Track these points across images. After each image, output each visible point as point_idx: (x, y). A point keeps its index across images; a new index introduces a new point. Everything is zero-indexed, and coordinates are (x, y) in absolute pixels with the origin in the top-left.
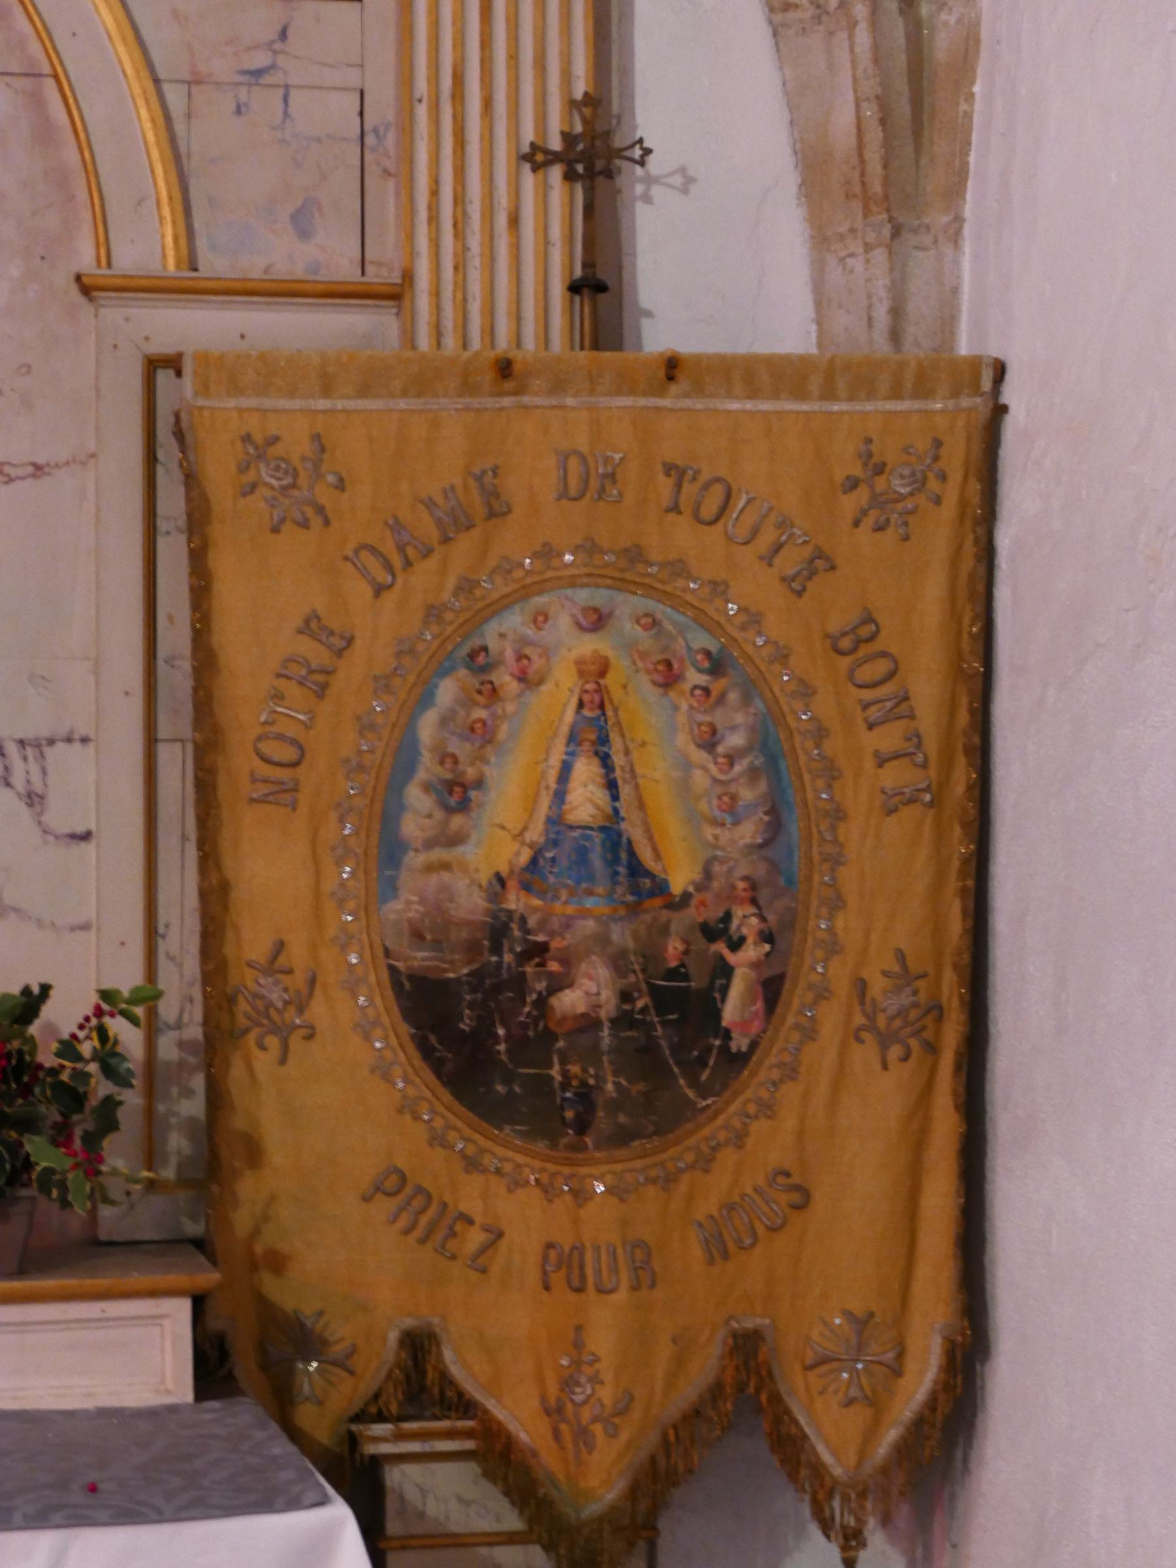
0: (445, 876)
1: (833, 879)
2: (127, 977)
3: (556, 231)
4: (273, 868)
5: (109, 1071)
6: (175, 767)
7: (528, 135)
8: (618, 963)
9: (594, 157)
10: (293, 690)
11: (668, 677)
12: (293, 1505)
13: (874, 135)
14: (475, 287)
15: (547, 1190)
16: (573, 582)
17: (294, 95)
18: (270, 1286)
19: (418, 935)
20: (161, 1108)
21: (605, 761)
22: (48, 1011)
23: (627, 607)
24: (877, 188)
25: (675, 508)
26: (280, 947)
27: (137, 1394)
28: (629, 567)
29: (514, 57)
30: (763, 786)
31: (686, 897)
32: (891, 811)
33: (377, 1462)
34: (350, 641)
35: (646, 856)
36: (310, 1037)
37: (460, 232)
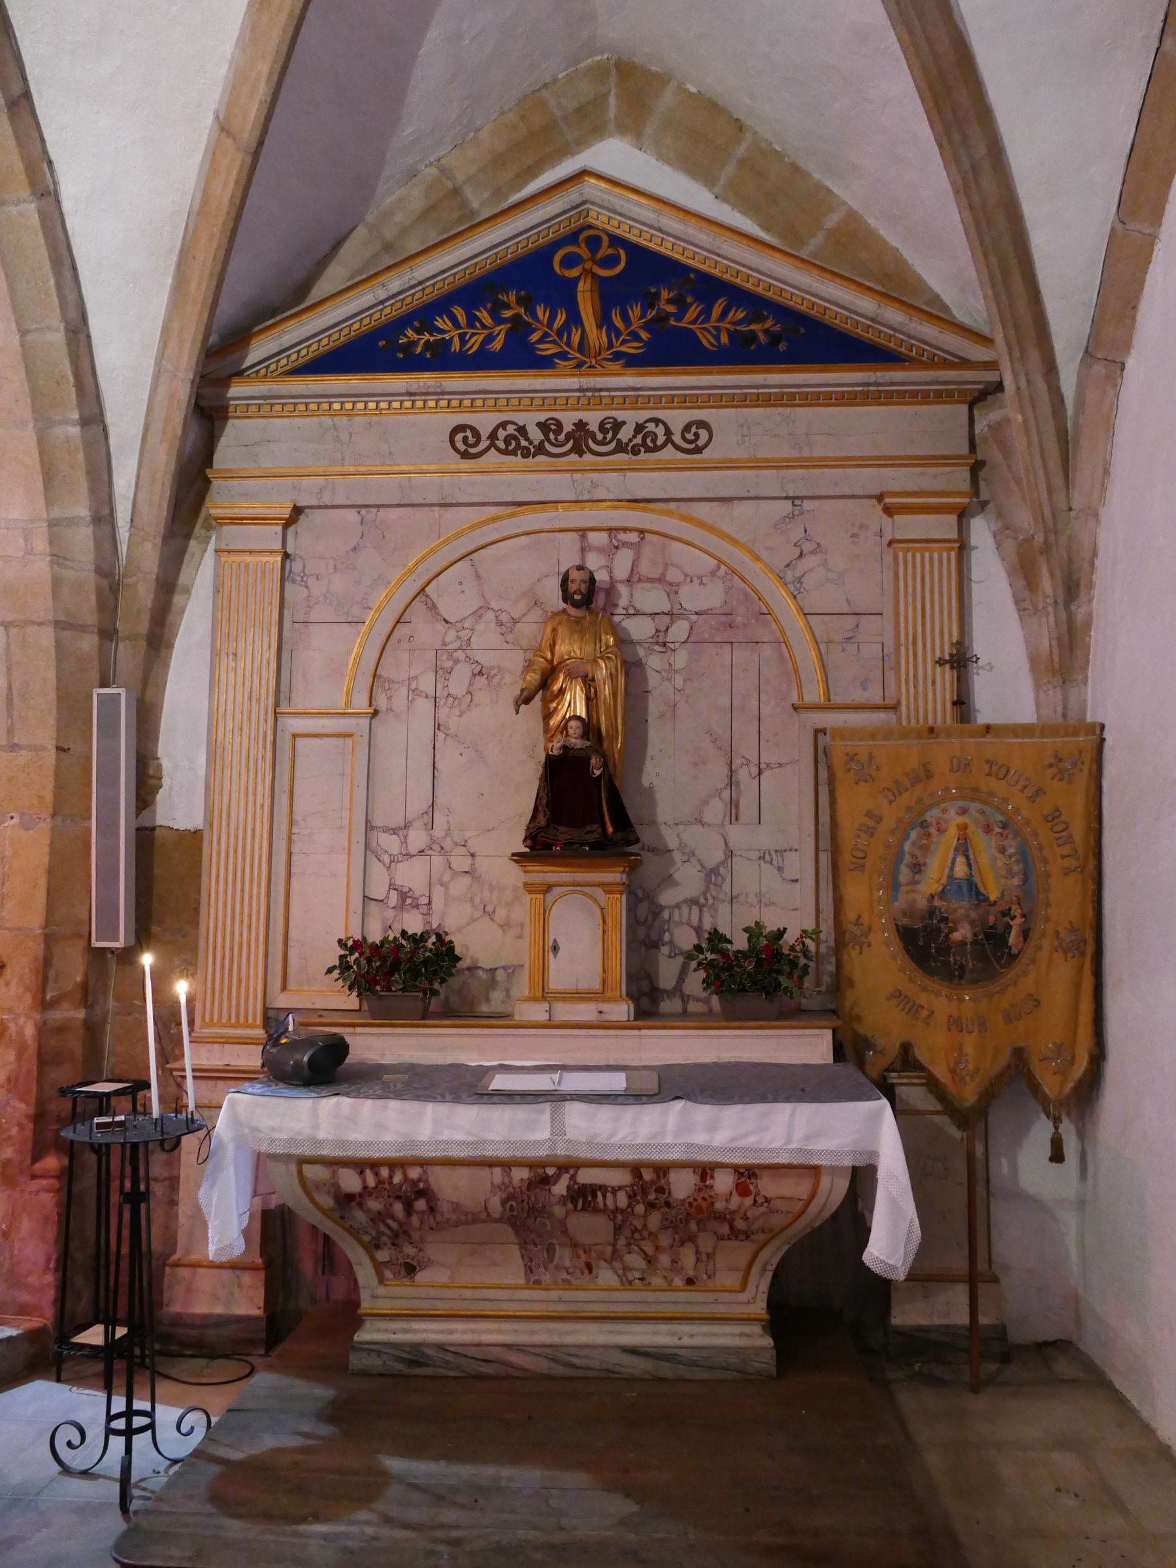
0: (914, 895)
1: (707, 889)
2: (810, 926)
3: (948, 685)
4: (856, 891)
5: (805, 956)
6: (825, 858)
7: (938, 655)
8: (972, 924)
9: (960, 661)
10: (864, 835)
11: (988, 829)
12: (869, 1099)
13: (1056, 651)
14: (921, 704)
15: (950, 999)
16: (955, 799)
17: (861, 645)
18: (856, 1026)
19: (905, 914)
20: (821, 967)
21: (967, 857)
22: (786, 936)
23: (974, 807)
24: (1057, 668)
25: (989, 775)
26: (859, 917)
27: (815, 1060)
28: (974, 794)
29: (933, 630)
30: (1021, 866)
31: (995, 902)
32: (1066, 874)
33: (892, 1085)
34: (881, 819)
35: (981, 888)
36: (869, 946)
37: (229, 999)
